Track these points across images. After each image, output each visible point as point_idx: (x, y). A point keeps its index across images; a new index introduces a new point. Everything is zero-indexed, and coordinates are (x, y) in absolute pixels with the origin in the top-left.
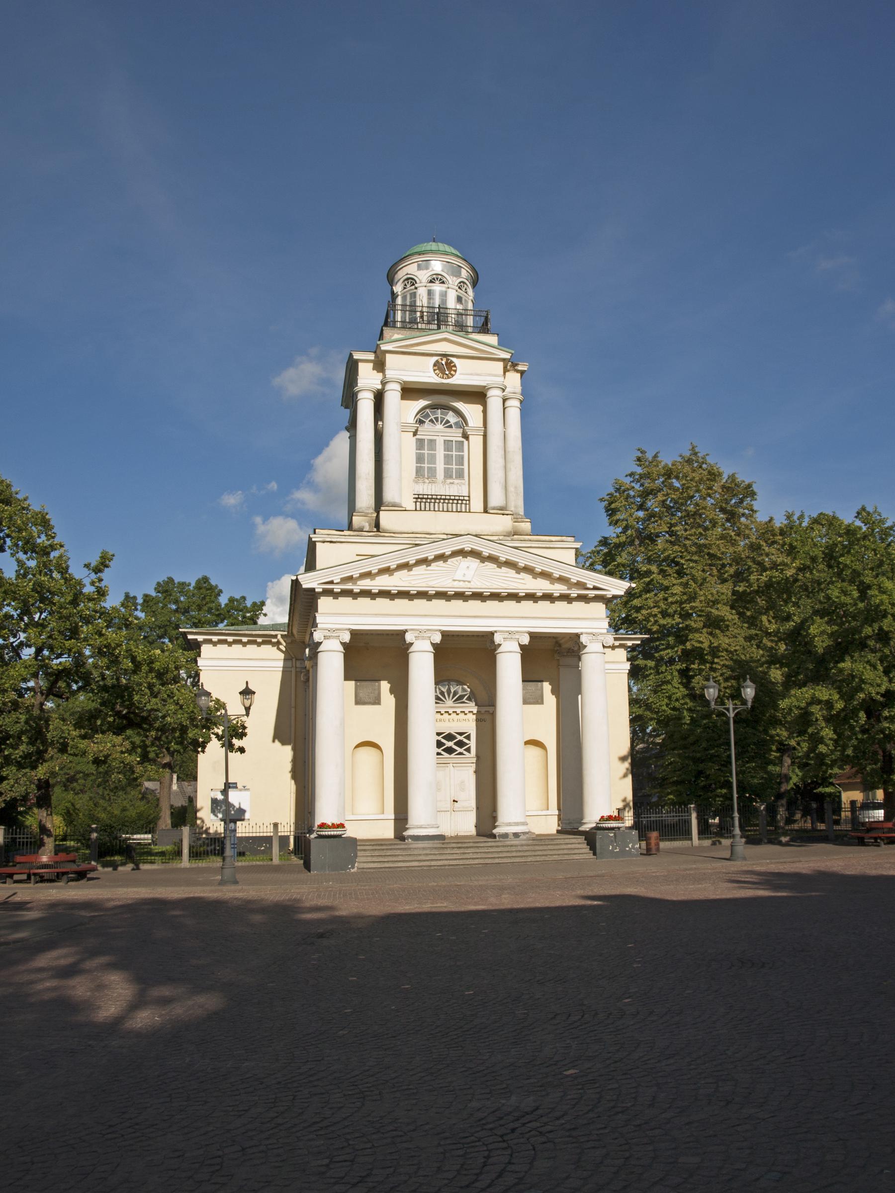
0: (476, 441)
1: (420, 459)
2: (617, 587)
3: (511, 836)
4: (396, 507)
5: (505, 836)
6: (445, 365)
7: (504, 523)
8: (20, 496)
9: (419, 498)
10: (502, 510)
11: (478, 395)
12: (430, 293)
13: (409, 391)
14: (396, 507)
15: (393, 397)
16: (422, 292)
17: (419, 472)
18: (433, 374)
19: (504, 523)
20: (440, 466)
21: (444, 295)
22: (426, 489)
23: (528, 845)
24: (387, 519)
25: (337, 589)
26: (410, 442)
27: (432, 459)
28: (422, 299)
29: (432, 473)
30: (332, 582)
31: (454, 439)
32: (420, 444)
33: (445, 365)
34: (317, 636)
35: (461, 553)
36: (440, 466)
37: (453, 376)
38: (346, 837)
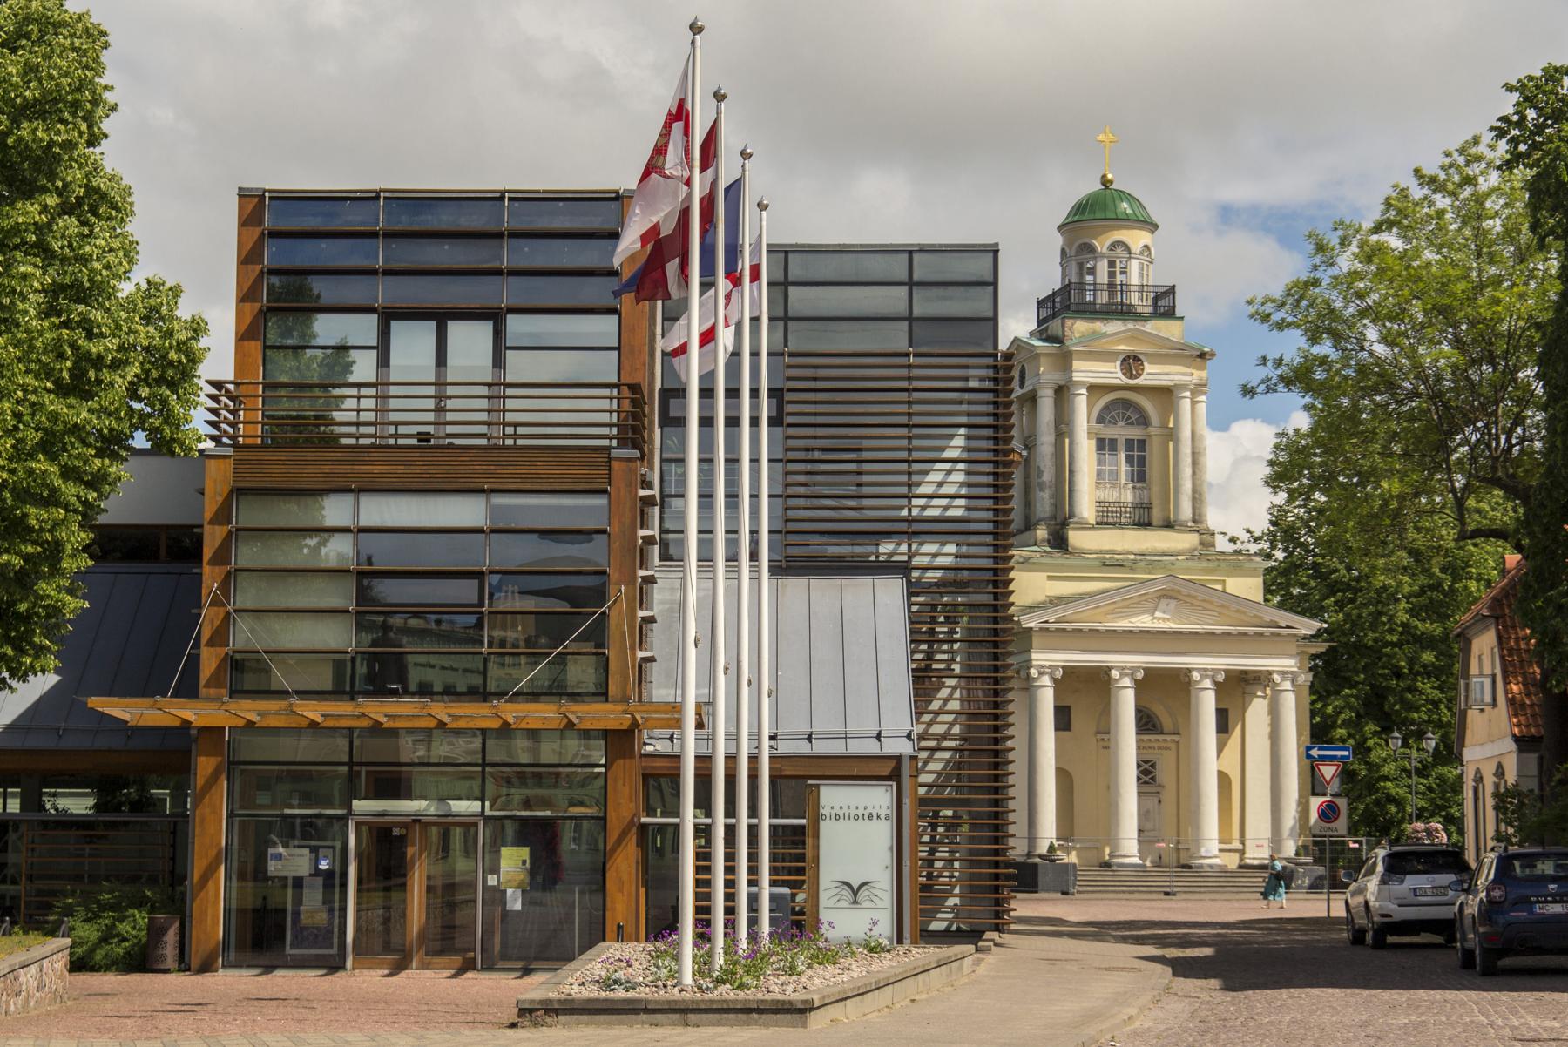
2: (1307, 626)
5: (1201, 866)
13: (1093, 389)
14: (1084, 526)
18: (1120, 374)
25: (1053, 626)
30: (1047, 622)
31: (1136, 438)
34: (1034, 672)
37: (1140, 375)
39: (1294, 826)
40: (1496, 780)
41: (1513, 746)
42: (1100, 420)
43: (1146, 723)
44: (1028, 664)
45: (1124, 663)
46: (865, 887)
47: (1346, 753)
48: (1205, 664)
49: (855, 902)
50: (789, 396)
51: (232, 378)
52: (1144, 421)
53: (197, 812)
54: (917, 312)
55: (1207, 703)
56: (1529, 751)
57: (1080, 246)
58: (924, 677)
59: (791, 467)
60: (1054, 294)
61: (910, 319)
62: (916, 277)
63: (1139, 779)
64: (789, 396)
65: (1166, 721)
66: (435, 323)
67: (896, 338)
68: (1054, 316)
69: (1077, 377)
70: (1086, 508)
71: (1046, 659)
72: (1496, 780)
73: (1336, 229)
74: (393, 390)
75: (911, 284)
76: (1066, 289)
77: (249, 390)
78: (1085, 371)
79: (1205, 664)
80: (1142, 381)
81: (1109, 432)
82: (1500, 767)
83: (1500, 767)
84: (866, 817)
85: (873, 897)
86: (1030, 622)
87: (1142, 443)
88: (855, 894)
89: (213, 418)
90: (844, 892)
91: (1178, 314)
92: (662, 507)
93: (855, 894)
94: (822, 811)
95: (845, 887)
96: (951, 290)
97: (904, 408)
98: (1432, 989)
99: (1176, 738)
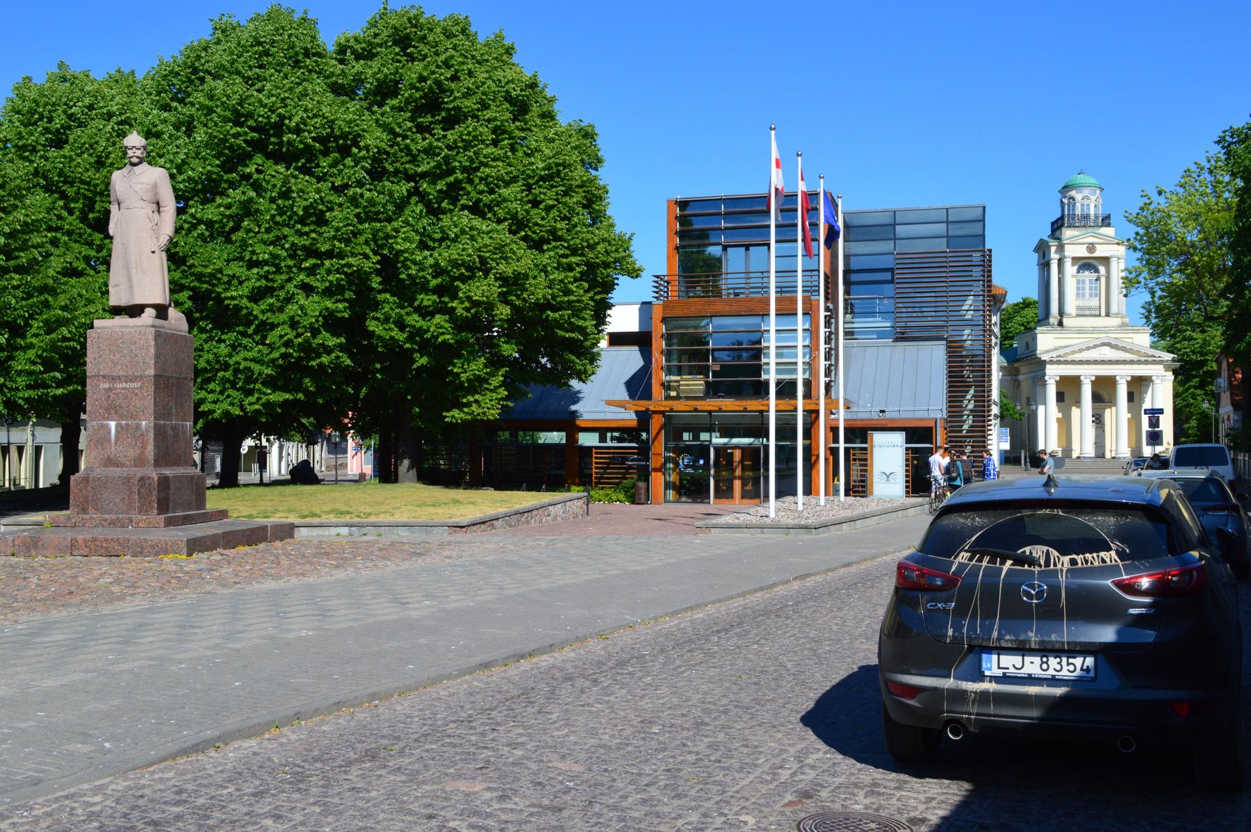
0: (1103, 280)
1: (1078, 289)
3: (686, 370)
4: (1070, 316)
6: (1091, 247)
7: (1116, 321)
8: (549, 93)
10: (1117, 315)
11: (1106, 260)
12: (1082, 205)
13: (1075, 260)
14: (1070, 316)
15: (1068, 263)
16: (1078, 205)
17: (1078, 295)
19: (1116, 321)
20: (1087, 292)
21: (1088, 205)
23: (266, 611)
24: (1065, 321)
26: (1074, 281)
27: (1084, 289)
28: (1078, 211)
29: (1084, 295)
32: (1078, 282)
33: (1091, 247)
34: (1046, 378)
35: (1104, 344)
36: (1087, 292)
38: (80, 430)
39: (1071, 481)
45: (1087, 374)
48: (1123, 374)
50: (896, 271)
51: (665, 273)
54: (950, 234)
55: (1122, 391)
59: (898, 300)
61: (895, 239)
62: (950, 219)
64: (896, 271)
67: (941, 245)
69: (1067, 254)
70: (1070, 307)
71: (1053, 373)
73: (1160, 193)
74: (751, 275)
75: (948, 222)
77: (673, 278)
78: (1072, 251)
79: (1123, 374)
80: (1095, 255)
86: (1044, 357)
92: (114, 379)
96: (965, 225)
97: (760, 280)
98: (844, 752)
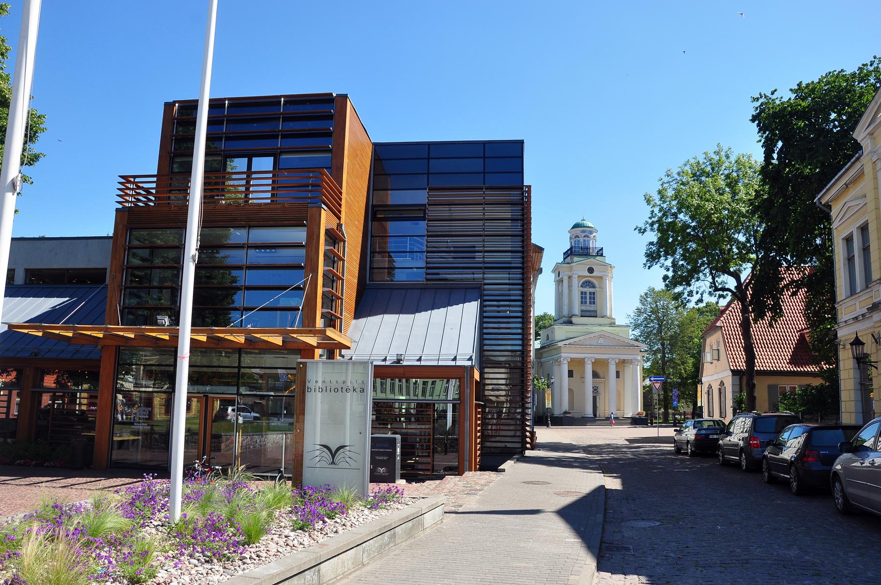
9: (582, 311)
12: (584, 241)
17: (582, 302)
22: (584, 308)
29: (586, 302)
30: (566, 344)
40: (720, 387)
41: (730, 373)
42: (582, 286)
43: (595, 375)
44: (560, 357)
46: (342, 450)
47: (663, 379)
49: (333, 463)
52: (594, 287)
53: (243, 393)
55: (612, 369)
56: (736, 375)
57: (586, 282)
58: (371, 268)
60: (568, 250)
63: (593, 392)
65: (601, 375)
66: (253, 158)
68: (568, 256)
72: (720, 387)
76: (571, 249)
81: (584, 290)
82: (722, 383)
83: (722, 383)
84: (344, 390)
85: (348, 459)
86: (560, 344)
87: (594, 293)
88: (333, 456)
89: (122, 187)
90: (324, 454)
91: (604, 255)
93: (333, 456)
94: (308, 384)
95: (325, 449)
99: (605, 379)
